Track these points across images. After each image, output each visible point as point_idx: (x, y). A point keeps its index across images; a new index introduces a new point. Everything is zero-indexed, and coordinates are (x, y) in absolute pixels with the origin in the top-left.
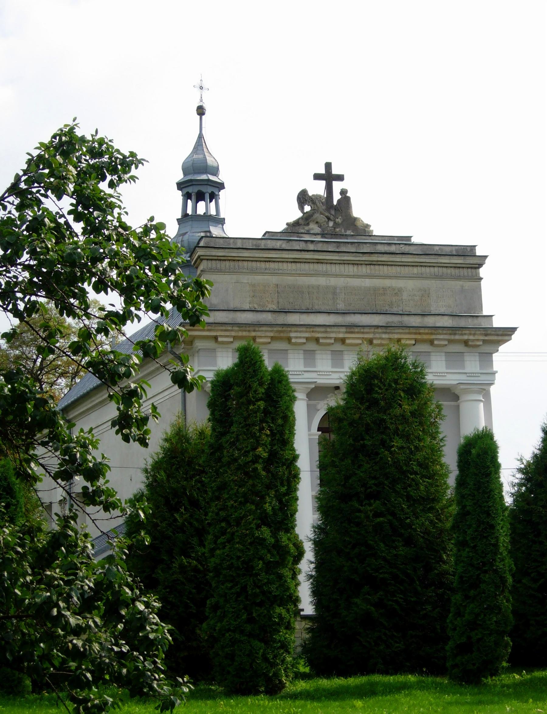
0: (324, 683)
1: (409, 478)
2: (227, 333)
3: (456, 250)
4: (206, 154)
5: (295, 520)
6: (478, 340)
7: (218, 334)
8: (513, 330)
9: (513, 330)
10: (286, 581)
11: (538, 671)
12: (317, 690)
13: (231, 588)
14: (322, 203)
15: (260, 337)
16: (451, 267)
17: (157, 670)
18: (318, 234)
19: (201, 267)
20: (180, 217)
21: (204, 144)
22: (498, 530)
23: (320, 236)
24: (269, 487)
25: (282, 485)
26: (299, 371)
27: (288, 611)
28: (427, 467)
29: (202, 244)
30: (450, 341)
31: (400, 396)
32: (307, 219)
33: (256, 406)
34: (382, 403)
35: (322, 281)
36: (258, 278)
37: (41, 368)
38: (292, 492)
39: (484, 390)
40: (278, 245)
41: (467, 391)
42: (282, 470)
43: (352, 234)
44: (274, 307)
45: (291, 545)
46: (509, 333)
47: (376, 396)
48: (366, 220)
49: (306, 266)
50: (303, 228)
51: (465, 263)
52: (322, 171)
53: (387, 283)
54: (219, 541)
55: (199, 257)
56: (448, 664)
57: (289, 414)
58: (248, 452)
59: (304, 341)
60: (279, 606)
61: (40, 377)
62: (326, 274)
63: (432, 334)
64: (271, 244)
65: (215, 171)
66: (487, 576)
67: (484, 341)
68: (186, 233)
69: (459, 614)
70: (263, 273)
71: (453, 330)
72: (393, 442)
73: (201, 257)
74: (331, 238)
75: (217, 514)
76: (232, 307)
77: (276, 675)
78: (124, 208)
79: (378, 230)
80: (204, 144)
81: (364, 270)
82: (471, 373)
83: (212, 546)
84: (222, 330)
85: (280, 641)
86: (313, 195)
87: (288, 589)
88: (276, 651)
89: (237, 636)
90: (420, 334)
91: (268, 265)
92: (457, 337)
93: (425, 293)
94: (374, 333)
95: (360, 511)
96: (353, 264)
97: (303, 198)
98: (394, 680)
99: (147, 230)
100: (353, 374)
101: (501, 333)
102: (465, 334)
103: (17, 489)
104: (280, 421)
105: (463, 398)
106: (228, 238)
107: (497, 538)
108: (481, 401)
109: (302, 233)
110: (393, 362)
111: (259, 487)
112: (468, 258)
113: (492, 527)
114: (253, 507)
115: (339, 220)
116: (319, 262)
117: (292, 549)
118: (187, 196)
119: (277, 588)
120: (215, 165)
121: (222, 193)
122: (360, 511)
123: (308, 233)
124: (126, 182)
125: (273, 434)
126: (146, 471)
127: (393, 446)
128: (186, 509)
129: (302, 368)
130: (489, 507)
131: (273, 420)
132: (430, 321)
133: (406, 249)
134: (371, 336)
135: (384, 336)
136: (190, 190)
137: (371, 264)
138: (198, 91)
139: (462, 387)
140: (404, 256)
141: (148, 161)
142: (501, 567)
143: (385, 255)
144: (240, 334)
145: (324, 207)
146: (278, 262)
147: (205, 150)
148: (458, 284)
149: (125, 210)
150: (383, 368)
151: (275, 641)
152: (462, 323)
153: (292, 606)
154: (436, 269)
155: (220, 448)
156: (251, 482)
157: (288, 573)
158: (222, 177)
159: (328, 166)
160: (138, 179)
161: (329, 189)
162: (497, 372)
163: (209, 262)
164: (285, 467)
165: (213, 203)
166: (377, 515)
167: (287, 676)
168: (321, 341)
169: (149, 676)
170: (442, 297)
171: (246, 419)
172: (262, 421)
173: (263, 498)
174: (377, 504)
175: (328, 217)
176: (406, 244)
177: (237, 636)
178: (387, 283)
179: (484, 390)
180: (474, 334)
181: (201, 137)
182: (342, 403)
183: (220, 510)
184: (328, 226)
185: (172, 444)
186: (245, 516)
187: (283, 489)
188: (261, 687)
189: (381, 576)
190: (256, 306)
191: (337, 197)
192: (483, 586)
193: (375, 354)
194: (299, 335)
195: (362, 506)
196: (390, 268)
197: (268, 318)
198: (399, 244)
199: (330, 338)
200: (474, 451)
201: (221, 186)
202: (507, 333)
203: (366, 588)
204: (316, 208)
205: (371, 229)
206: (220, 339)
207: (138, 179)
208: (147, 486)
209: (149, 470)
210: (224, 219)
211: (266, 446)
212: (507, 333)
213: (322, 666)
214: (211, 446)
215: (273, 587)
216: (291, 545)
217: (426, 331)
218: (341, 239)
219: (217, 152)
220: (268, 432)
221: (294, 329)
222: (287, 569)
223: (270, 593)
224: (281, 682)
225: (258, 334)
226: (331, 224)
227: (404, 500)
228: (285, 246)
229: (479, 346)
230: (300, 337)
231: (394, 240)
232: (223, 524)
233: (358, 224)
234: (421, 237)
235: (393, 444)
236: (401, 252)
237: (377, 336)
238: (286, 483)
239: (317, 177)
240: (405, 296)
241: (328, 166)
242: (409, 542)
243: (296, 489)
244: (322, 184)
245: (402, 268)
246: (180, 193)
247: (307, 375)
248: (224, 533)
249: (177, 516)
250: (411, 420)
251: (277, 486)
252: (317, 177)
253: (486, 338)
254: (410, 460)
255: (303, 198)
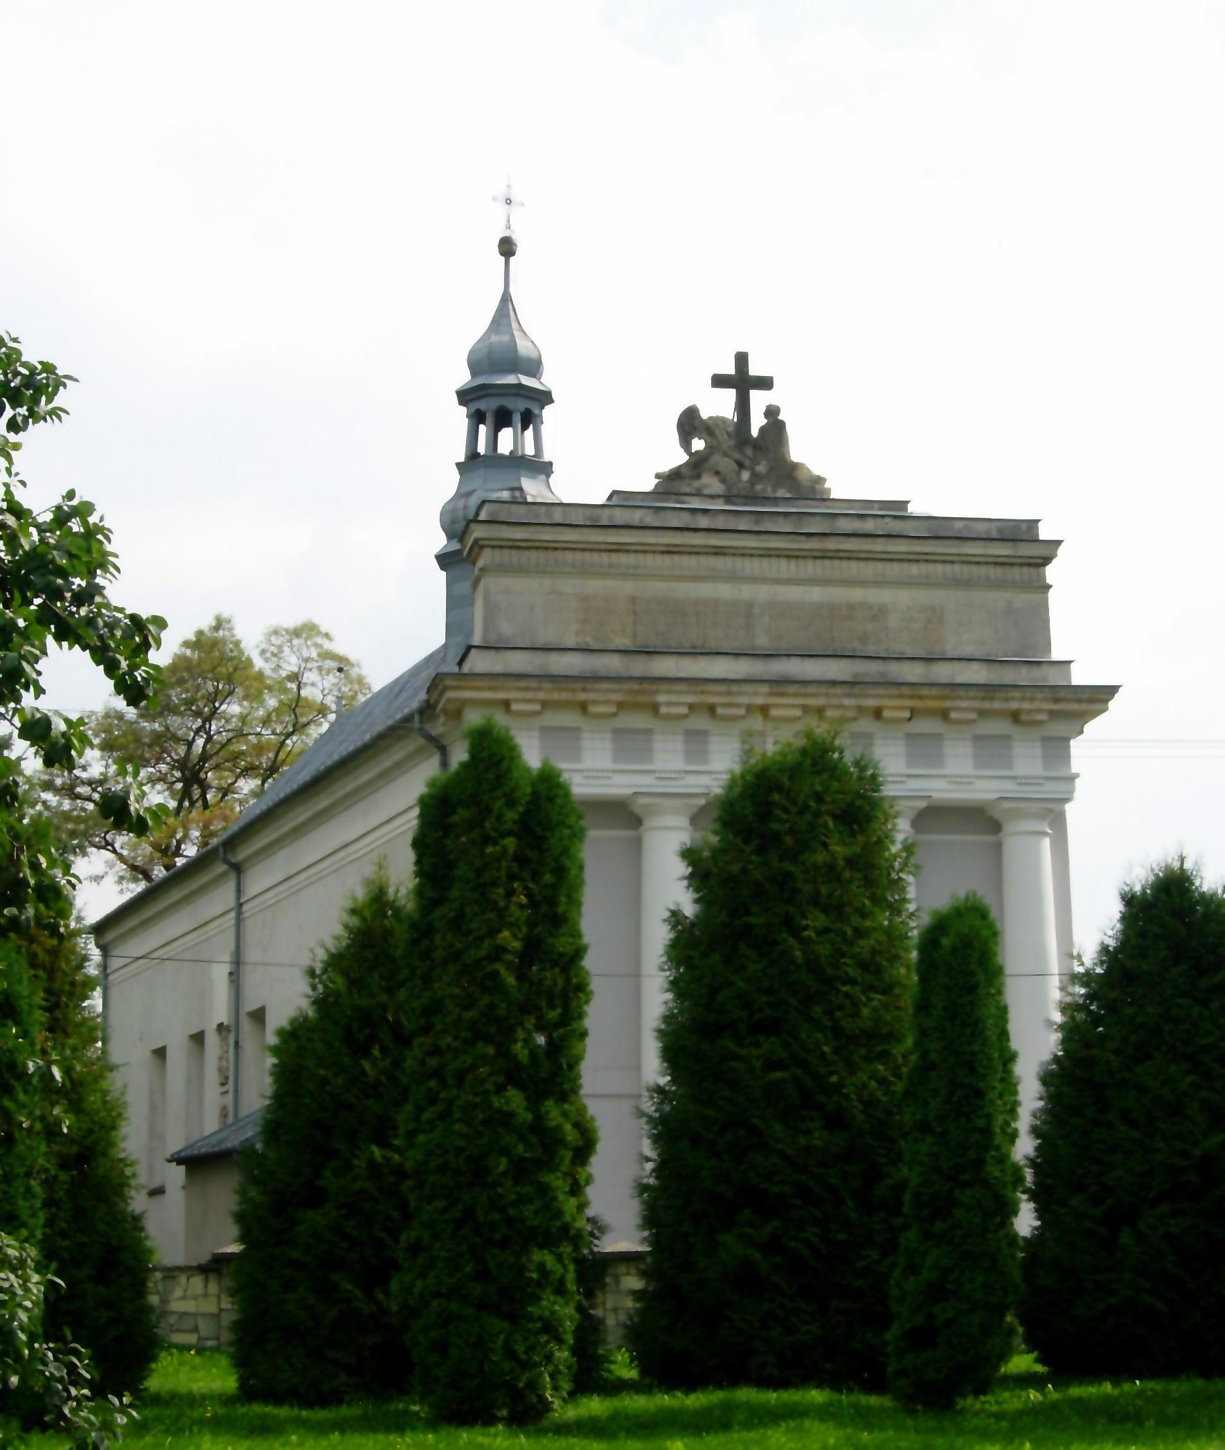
0: (665, 1400)
1: (838, 991)
2: (530, 695)
3: (1000, 530)
4: (517, 334)
5: (579, 1076)
6: (1039, 711)
7: (511, 695)
8: (1112, 690)
9: (1112, 690)
10: (555, 1198)
11: (1081, 1384)
12: (614, 1416)
13: (444, 1210)
14: (728, 433)
15: (596, 703)
16: (987, 563)
17: (76, 1380)
18: (718, 496)
19: (481, 563)
20: (462, 459)
21: (512, 313)
22: (991, 1101)
23: (721, 501)
24: (525, 1009)
25: (552, 1006)
26: (676, 772)
27: (560, 1258)
28: (878, 971)
29: (482, 517)
30: (983, 714)
31: (826, 826)
32: (697, 464)
33: (498, 848)
34: (788, 840)
35: (724, 591)
36: (595, 585)
37: (204, 757)
38: (573, 1019)
39: (1052, 815)
40: (636, 517)
41: (1017, 814)
42: (552, 976)
43: (788, 495)
44: (623, 642)
45: (568, 1127)
46: (1103, 697)
47: (775, 826)
48: (816, 470)
49: (692, 561)
50: (689, 485)
51: (1014, 555)
52: (730, 369)
53: (857, 595)
54: (426, 1116)
55: (476, 541)
56: (891, 1368)
57: (567, 863)
58: (481, 939)
59: (685, 710)
60: (541, 1247)
61: (202, 775)
62: (732, 578)
63: (944, 698)
64: (621, 516)
65: (534, 367)
66: (968, 1193)
67: (1053, 714)
68: (473, 492)
69: (912, 1269)
70: (604, 575)
71: (989, 690)
72: (806, 918)
73: (482, 543)
74: (745, 504)
75: (423, 1063)
76: (541, 640)
77: (533, 1385)
78: (17, 474)
79: (841, 487)
80: (512, 313)
81: (810, 568)
82: (1026, 778)
83: (411, 1126)
84: (518, 689)
85: (541, 1318)
86: (710, 418)
87: (559, 1214)
88: (532, 1338)
89: (454, 1306)
90: (920, 697)
91: (614, 558)
92: (997, 705)
93: (935, 617)
94: (827, 695)
95: (736, 1057)
96: (788, 557)
97: (690, 424)
98: (778, 1398)
99: (61, 517)
100: (733, 780)
101: (1085, 696)
102: (1013, 699)
103: (25, 1008)
104: (548, 878)
105: (1009, 827)
106: (561, 504)
107: (989, 1117)
108: (1046, 834)
109: (686, 494)
110: (817, 759)
111: (502, 1011)
112: (1021, 544)
113: (980, 1094)
114: (491, 1050)
115: (761, 468)
116: (718, 552)
117: (570, 1134)
118: (477, 418)
119: (536, 1213)
120: (534, 355)
121: (548, 412)
122: (736, 1057)
123: (698, 494)
124: (45, 420)
125: (533, 903)
126: (311, 973)
127: (806, 928)
128: (384, 1050)
129: (681, 766)
130: (974, 1054)
131: (535, 875)
132: (942, 672)
133: (897, 527)
134: (820, 702)
135: (847, 702)
136: (482, 405)
137: (824, 556)
138: (501, 209)
139: (1006, 805)
140: (891, 540)
141: (76, 380)
142: (997, 1174)
143: (853, 539)
144: (556, 696)
145: (732, 442)
146: (637, 552)
147: (514, 325)
148: (999, 598)
149: (19, 478)
150: (794, 771)
151: (531, 1318)
152: (1009, 676)
153: (569, 1249)
154: (957, 567)
155: (429, 930)
156: (486, 999)
157: (559, 1183)
158: (549, 380)
159: (742, 360)
160: (67, 413)
161: (743, 406)
162: (1077, 776)
163: (497, 552)
164: (557, 970)
165: (529, 433)
166: (772, 1065)
167: (556, 1388)
168: (720, 711)
169: (57, 1391)
170: (971, 623)
171: (479, 873)
172: (512, 877)
173: (511, 1030)
174: (771, 1045)
175: (739, 464)
176: (895, 517)
177: (454, 1306)
178: (857, 595)
179: (1051, 811)
180: (1032, 700)
181: (506, 299)
182: (714, 839)
183: (429, 1054)
184: (740, 481)
185: (364, 919)
186: (473, 1067)
187: (553, 1015)
188: (500, 1408)
189: (776, 1189)
190: (589, 640)
191: (757, 422)
192: (959, 1213)
193: (776, 741)
194: (674, 698)
195: (742, 1046)
196: (862, 564)
197: (612, 664)
198: (883, 516)
199: (738, 706)
200: (945, 941)
201: (545, 398)
202: (1098, 698)
203: (747, 1214)
204: (715, 443)
205: (827, 486)
206: (514, 707)
207: (67, 413)
208: (315, 1003)
209: (318, 972)
210: (551, 464)
211: (519, 928)
212: (1098, 698)
213: (666, 1368)
214: (414, 926)
215: (528, 1211)
216: (568, 1127)
217: (934, 691)
218: (764, 505)
219: (539, 331)
220: (523, 899)
221: (663, 687)
222: (559, 1174)
223: (523, 1221)
224: (542, 1399)
225: (592, 696)
226: (745, 476)
227: (826, 1037)
228: (650, 520)
229: (1041, 723)
230: (677, 704)
231: (872, 509)
232: (433, 1083)
233: (800, 476)
234: (931, 499)
235: (805, 922)
236: (887, 533)
237: (834, 701)
238: (558, 1002)
239: (719, 381)
240: (893, 621)
241: (742, 360)
242: (836, 1121)
243: (580, 1016)
244: (730, 395)
245: (888, 565)
246: (464, 410)
247: (691, 779)
248: (433, 1101)
249: (367, 1065)
250: (847, 874)
251: (540, 1009)
252: (719, 381)
253: (1057, 707)
254: (843, 955)
255: (690, 424)
